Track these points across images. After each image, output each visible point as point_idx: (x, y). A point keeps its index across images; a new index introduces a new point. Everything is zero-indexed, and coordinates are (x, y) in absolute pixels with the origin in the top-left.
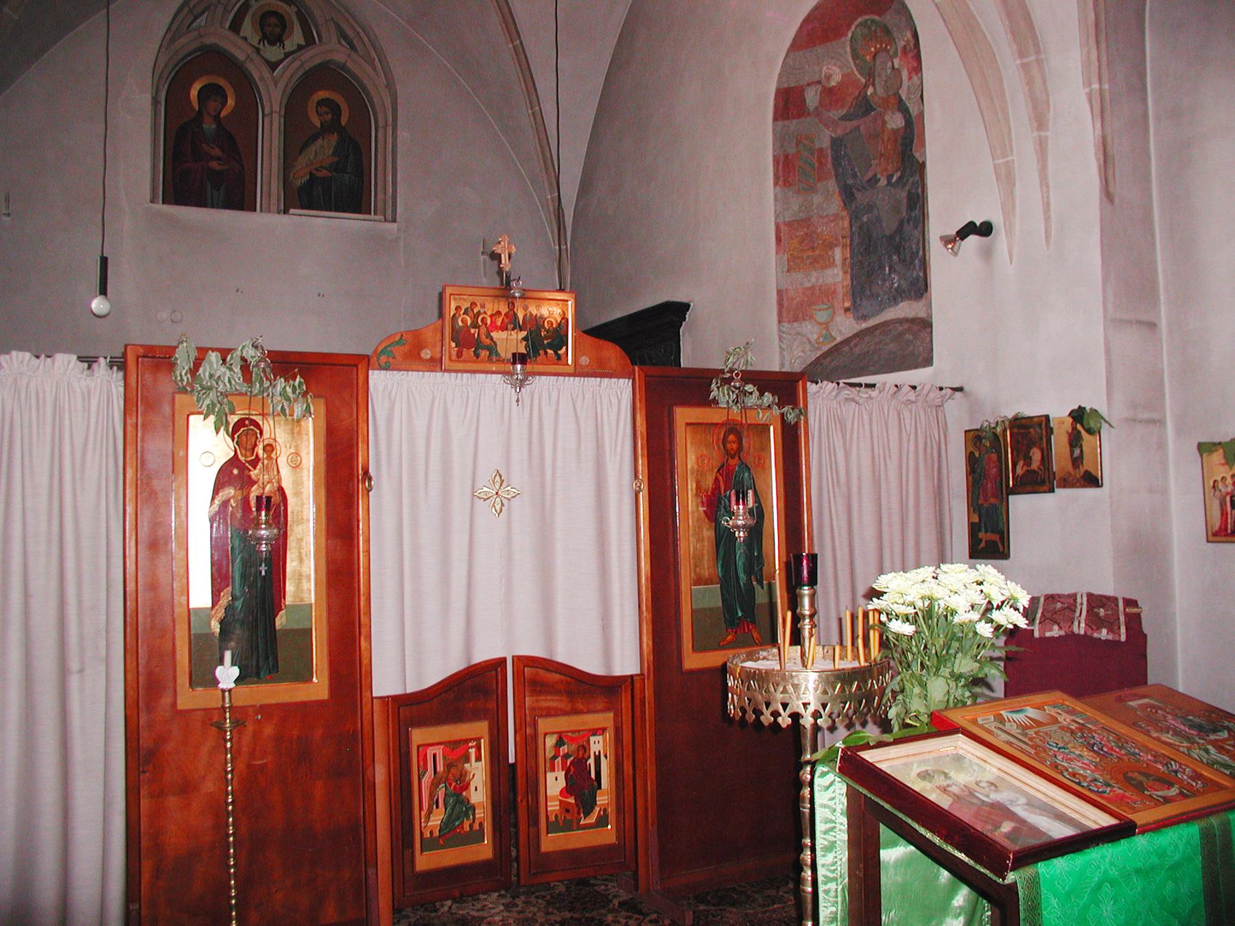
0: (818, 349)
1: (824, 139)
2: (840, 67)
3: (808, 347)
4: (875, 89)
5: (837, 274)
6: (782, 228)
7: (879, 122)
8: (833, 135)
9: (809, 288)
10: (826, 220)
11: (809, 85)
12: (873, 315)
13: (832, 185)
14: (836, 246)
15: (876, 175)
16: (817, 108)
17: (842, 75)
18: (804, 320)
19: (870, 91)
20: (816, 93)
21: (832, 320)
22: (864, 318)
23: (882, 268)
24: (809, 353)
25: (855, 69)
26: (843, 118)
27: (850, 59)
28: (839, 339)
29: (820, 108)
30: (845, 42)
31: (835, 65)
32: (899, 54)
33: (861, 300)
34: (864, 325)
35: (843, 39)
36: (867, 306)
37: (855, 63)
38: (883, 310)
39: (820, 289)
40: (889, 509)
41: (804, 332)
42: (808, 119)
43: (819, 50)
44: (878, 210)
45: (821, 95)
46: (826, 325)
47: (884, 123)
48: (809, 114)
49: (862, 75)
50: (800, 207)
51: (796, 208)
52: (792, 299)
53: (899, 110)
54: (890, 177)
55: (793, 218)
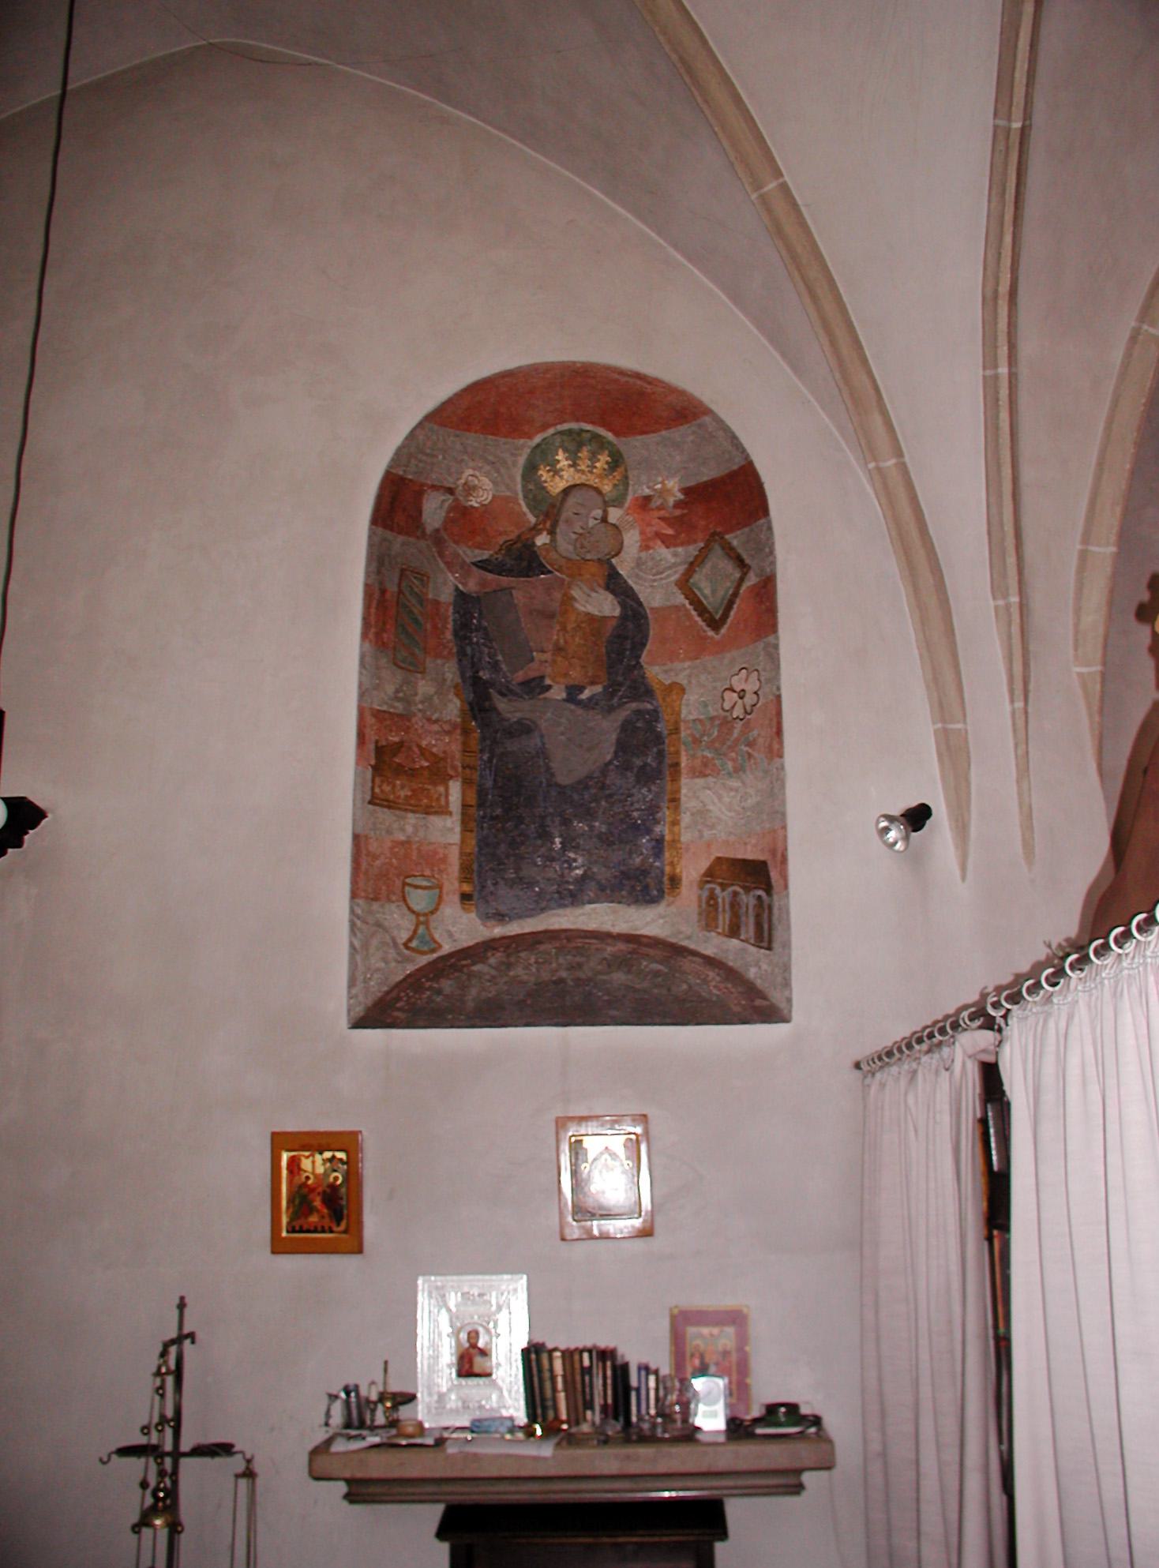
0: (408, 960)
1: (445, 586)
2: (495, 483)
3: (392, 953)
4: (553, 540)
5: (451, 830)
6: (368, 715)
7: (558, 595)
8: (461, 587)
9: (402, 843)
10: (436, 728)
11: (434, 487)
12: (520, 917)
13: (451, 671)
14: (451, 777)
15: (542, 678)
16: (437, 531)
17: (494, 497)
18: (389, 900)
19: (542, 540)
20: (441, 507)
21: (436, 909)
22: (501, 917)
23: (545, 835)
24: (393, 964)
25: (521, 496)
26: (482, 565)
27: (519, 479)
28: (447, 948)
29: (442, 532)
30: (523, 446)
31: (487, 474)
32: (627, 505)
33: (496, 884)
34: (498, 931)
35: (522, 441)
36: (507, 897)
37: (524, 487)
38: (543, 910)
39: (419, 849)
40: (422, 1344)
41: (386, 924)
42: (422, 544)
43: (473, 440)
44: (542, 736)
45: (448, 512)
46: (423, 919)
47: (568, 599)
48: (424, 535)
49: (532, 509)
50: (397, 691)
51: (390, 689)
52: (375, 857)
53: (607, 588)
54: (573, 691)
55: (385, 708)
